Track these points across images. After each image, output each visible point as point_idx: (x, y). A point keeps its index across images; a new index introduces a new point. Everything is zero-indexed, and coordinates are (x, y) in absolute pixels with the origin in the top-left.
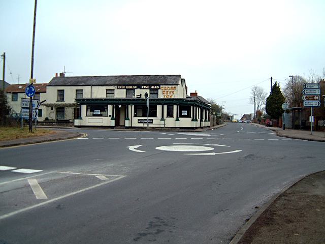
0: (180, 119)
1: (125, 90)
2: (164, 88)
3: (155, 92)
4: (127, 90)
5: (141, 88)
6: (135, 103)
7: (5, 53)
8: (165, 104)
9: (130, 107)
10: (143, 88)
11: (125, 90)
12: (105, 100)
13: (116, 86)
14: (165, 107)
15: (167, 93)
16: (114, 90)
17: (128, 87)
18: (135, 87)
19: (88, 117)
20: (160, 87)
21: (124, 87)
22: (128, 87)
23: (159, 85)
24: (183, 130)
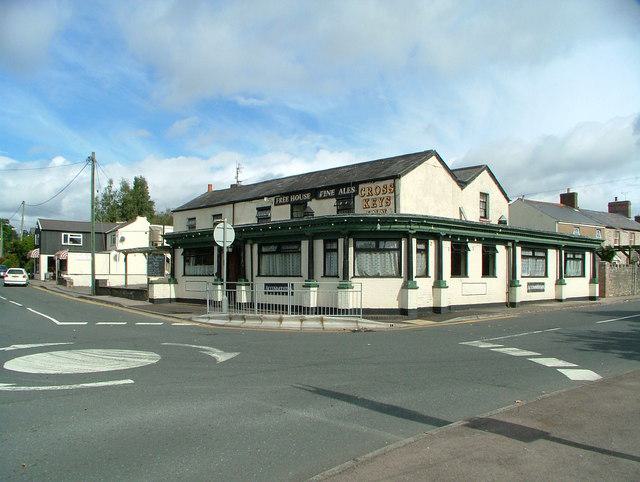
0: (567, 280)
1: (334, 200)
2: (367, 192)
3: (345, 203)
4: (293, 205)
5: (317, 198)
6: (455, 237)
7: (93, 153)
8: (446, 237)
9: (248, 248)
10: (323, 198)
11: (334, 200)
12: (294, 225)
13: (273, 199)
14: (447, 246)
15: (374, 206)
16: (269, 208)
17: (294, 198)
18: (307, 196)
19: (187, 278)
20: (357, 189)
21: (332, 191)
22: (294, 198)
23: (356, 184)
24: (186, 305)
